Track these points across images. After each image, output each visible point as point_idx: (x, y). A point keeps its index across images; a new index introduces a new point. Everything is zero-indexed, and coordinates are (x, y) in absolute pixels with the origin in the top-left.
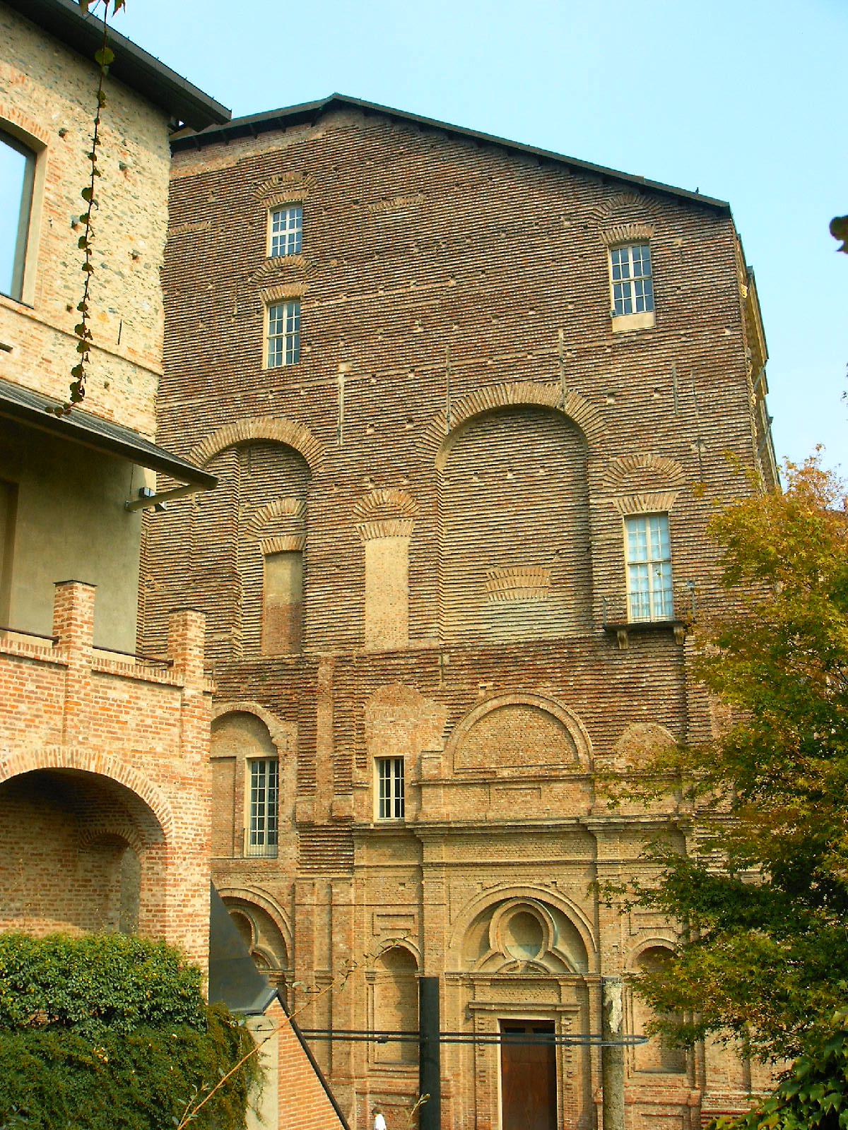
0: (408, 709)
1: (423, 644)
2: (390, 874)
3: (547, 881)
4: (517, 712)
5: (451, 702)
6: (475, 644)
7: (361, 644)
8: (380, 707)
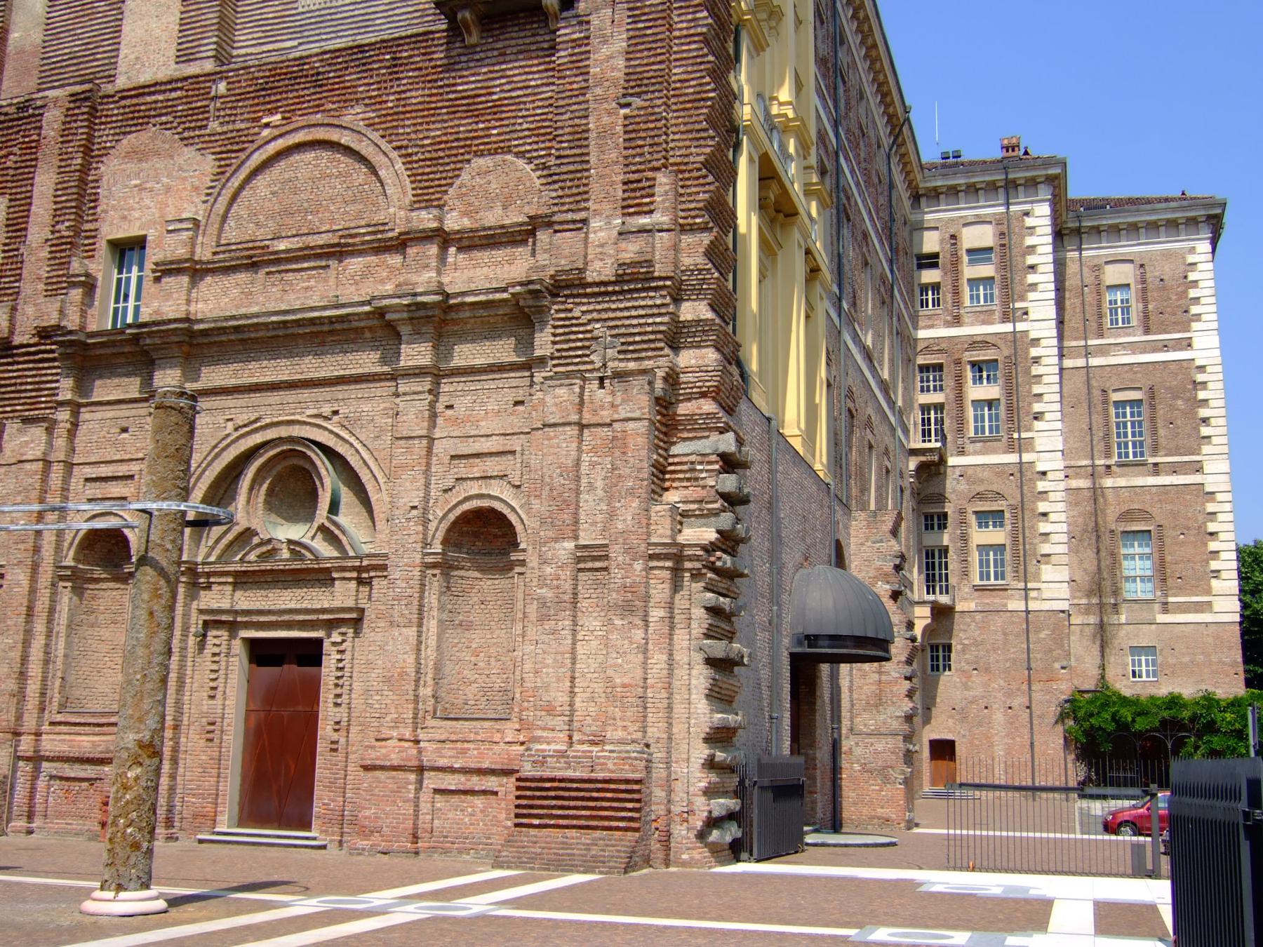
0: (160, 164)
1: (192, 69)
2: (110, 414)
3: (327, 410)
4: (309, 156)
5: (218, 150)
6: (264, 61)
7: (111, 78)
8: (123, 166)
